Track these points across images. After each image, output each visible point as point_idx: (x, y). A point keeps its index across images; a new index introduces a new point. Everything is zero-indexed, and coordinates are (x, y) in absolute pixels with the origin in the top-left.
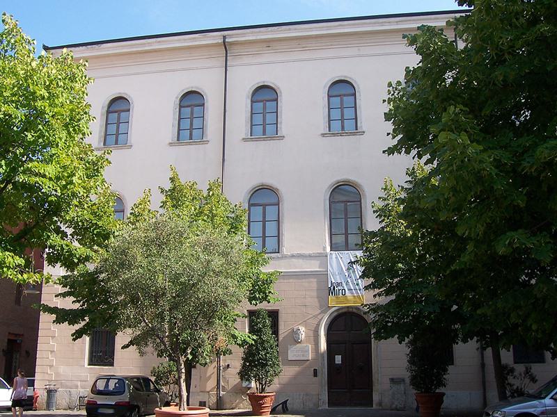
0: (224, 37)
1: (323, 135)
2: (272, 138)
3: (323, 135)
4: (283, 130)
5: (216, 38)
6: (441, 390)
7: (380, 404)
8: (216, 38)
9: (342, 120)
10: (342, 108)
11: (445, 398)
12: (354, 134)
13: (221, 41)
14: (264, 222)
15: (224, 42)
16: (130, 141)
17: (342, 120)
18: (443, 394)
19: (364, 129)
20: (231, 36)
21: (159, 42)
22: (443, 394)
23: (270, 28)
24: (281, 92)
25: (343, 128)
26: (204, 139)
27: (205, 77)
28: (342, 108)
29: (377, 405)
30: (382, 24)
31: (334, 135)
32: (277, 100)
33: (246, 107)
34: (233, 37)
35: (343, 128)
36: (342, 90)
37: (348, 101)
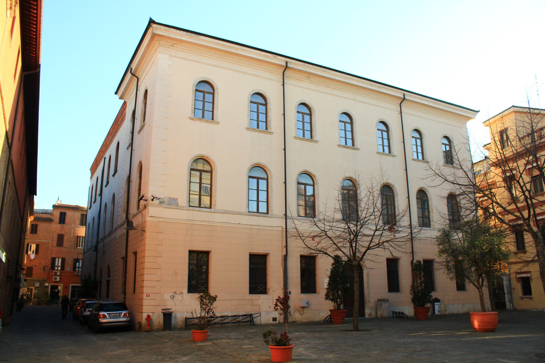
5: (400, 94)
7: (370, 315)
30: (440, 105)
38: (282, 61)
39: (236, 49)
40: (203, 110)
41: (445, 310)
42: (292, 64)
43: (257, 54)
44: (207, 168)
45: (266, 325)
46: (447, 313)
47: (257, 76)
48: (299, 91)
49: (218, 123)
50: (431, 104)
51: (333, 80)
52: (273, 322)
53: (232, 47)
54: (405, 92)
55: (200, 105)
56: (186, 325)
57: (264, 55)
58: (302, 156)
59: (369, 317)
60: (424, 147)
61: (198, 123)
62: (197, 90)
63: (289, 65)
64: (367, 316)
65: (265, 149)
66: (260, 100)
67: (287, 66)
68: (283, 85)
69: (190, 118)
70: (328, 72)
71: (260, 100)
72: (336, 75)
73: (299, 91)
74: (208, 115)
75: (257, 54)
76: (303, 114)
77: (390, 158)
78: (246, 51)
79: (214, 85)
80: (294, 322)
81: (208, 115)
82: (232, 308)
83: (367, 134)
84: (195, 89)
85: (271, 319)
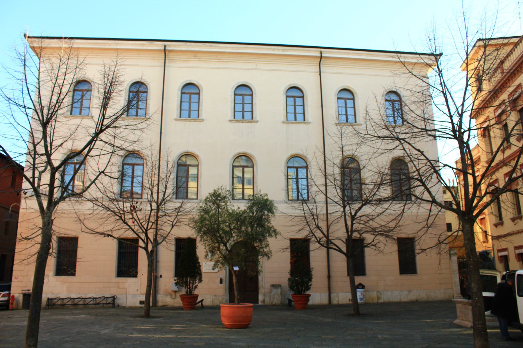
0: (165, 46)
1: (283, 122)
2: (195, 120)
3: (283, 122)
4: (204, 114)
5: (316, 53)
6: (308, 292)
7: (264, 301)
8: (160, 46)
9: (243, 111)
10: (243, 104)
11: (310, 298)
12: (250, 122)
13: (163, 48)
14: (297, 179)
15: (165, 50)
16: (256, 118)
17: (243, 111)
18: (309, 295)
19: (258, 119)
20: (170, 46)
21: (117, 43)
22: (309, 295)
23: (198, 44)
24: (202, 89)
25: (243, 117)
26: (147, 117)
27: (305, 77)
28: (190, 103)
29: (261, 302)
30: (374, 55)
31: (237, 121)
32: (199, 94)
33: (178, 97)
34: (171, 46)
35: (243, 117)
36: (243, 91)
37: (194, 98)
38: (316, 53)
39: (110, 44)
40: (295, 113)
41: (378, 298)
42: (326, 53)
43: (132, 44)
44: (194, 162)
45: (131, 308)
46: (381, 301)
47: (138, 66)
48: (336, 78)
49: (203, 120)
50: (281, 53)
51: (225, 53)
52: (141, 305)
53: (106, 44)
54: (322, 50)
55: (291, 109)
56: (148, 308)
57: (140, 44)
58: (180, 138)
59: (262, 304)
60: (356, 108)
61: (181, 124)
62: (338, 98)
63: (323, 55)
64: (260, 303)
65: (305, 139)
66: (295, 93)
67: (321, 56)
68: (320, 74)
69: (175, 119)
70: (215, 46)
71: (394, 97)
72: (226, 48)
73: (336, 78)
74: (300, 117)
75: (132, 44)
76: (346, 99)
77: (302, 127)
78: (120, 44)
79: (353, 91)
80: (164, 306)
81: (300, 117)
82: (97, 290)
83: (270, 102)
84: (336, 98)
85: (139, 302)
